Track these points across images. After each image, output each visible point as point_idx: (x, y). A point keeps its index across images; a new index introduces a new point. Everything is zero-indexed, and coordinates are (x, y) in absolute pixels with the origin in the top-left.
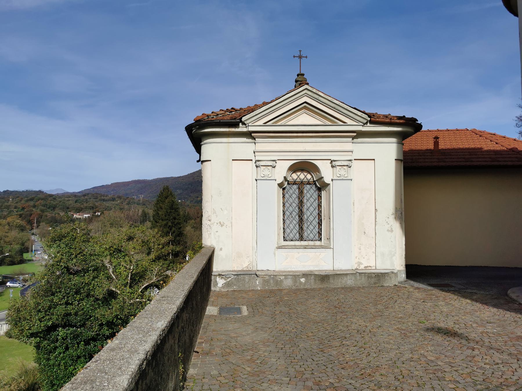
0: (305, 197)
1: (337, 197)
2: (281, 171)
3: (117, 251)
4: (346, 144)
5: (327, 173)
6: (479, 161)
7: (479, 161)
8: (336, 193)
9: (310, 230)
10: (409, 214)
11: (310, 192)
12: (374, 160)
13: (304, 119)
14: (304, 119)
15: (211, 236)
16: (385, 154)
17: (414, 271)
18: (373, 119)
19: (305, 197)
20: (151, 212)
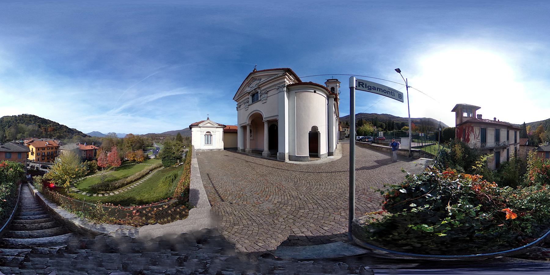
0: (209, 135)
1: (213, 137)
2: (205, 133)
3: (175, 145)
4: (215, 129)
5: (212, 133)
6: (36, 219)
7: (36, 219)
8: (213, 137)
9: (209, 142)
10: (224, 140)
11: (209, 136)
13: (209, 125)
14: (209, 125)
15: (193, 143)
16: (221, 130)
17: (225, 149)
18: (219, 125)
19: (209, 135)
20: (176, 138)
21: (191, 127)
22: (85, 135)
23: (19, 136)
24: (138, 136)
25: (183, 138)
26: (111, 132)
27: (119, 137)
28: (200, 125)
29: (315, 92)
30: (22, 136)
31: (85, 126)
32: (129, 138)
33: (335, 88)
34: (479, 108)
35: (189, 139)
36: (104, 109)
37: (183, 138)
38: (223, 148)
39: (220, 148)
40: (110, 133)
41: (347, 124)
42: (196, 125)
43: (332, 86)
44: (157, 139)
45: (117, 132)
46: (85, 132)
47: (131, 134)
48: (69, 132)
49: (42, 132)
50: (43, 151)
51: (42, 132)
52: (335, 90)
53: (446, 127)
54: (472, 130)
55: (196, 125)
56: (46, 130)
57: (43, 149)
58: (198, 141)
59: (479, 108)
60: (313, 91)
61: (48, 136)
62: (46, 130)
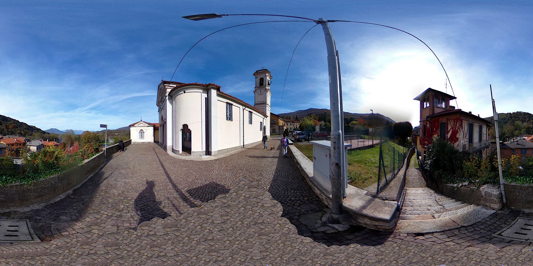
0: (142, 132)
5: (144, 131)
14: (142, 125)
16: (152, 128)
17: (154, 142)
19: (142, 132)
21: (130, 126)
22: (44, 132)
23: (517, 132)
24: (94, 133)
25: (126, 132)
26: (69, 129)
27: (76, 133)
28: (135, 125)
29: (185, 92)
30: (519, 132)
31: (43, 122)
32: (86, 135)
34: (454, 98)
35: (129, 134)
36: (72, 107)
37: (126, 132)
38: (153, 141)
39: (150, 141)
40: (67, 130)
41: (297, 118)
42: (133, 125)
43: (261, 77)
44: (112, 135)
45: (73, 130)
46: (43, 129)
47: (88, 131)
48: (28, 129)
49: (3, 129)
50: (12, 147)
51: (3, 129)
52: (264, 80)
53: (394, 124)
54: (461, 125)
55: (133, 125)
56: (7, 127)
57: (13, 145)
58: (135, 137)
59: (454, 98)
60: (183, 92)
61: (10, 133)
62: (7, 127)
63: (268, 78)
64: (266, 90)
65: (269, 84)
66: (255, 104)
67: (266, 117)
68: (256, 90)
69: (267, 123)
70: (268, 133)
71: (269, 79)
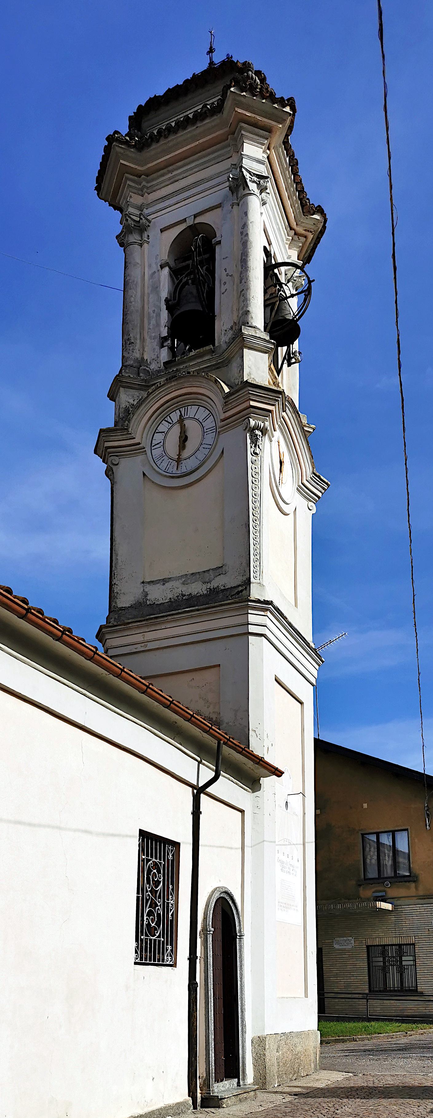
12: (242, 811)
33: (224, 233)
63: (267, 226)
64: (244, 409)
65: (282, 330)
66: (120, 617)
67: (227, 750)
68: (124, 419)
69: (265, 854)
70: (281, 994)
71: (285, 252)
